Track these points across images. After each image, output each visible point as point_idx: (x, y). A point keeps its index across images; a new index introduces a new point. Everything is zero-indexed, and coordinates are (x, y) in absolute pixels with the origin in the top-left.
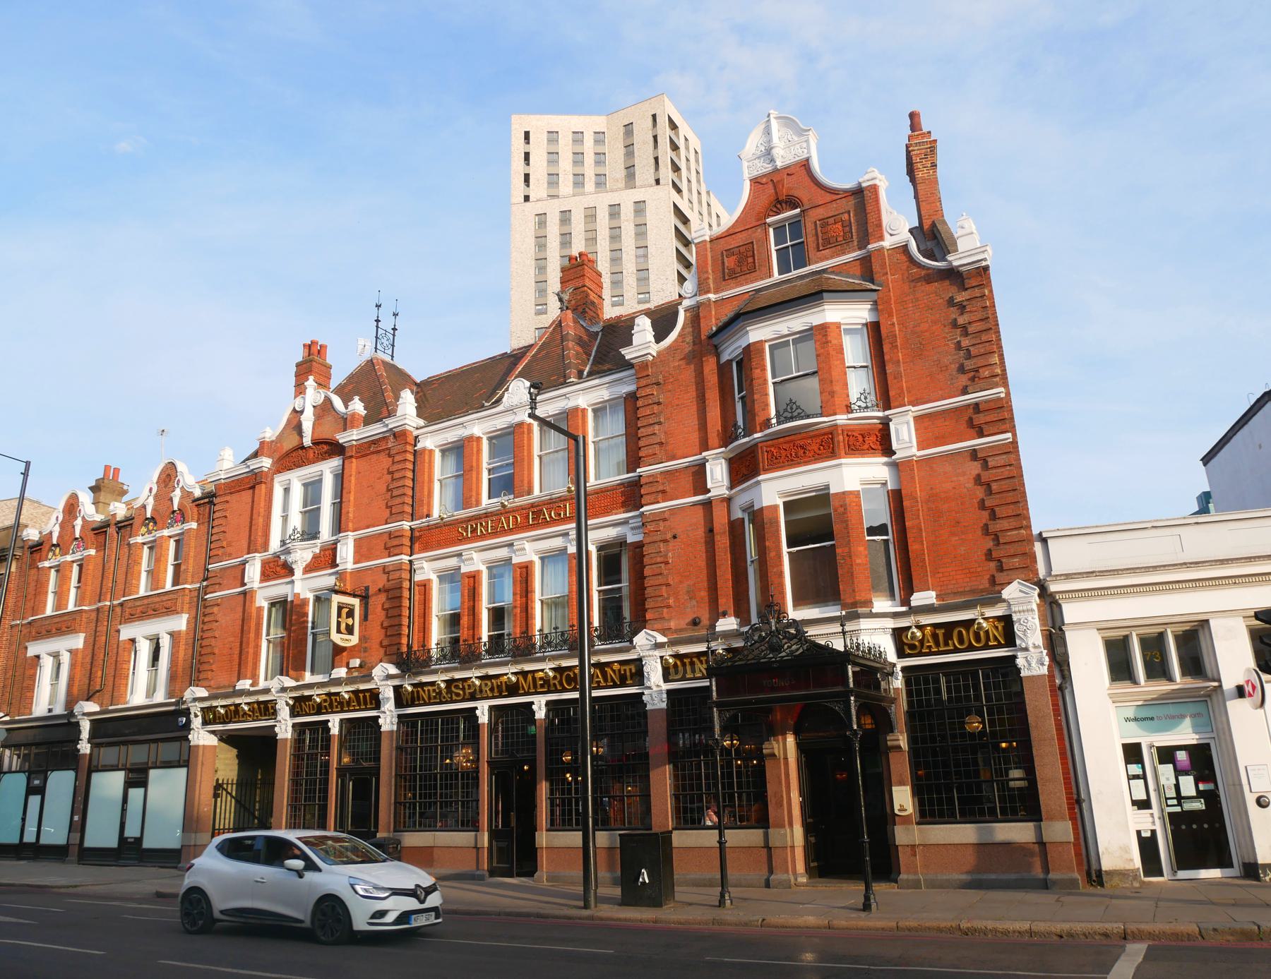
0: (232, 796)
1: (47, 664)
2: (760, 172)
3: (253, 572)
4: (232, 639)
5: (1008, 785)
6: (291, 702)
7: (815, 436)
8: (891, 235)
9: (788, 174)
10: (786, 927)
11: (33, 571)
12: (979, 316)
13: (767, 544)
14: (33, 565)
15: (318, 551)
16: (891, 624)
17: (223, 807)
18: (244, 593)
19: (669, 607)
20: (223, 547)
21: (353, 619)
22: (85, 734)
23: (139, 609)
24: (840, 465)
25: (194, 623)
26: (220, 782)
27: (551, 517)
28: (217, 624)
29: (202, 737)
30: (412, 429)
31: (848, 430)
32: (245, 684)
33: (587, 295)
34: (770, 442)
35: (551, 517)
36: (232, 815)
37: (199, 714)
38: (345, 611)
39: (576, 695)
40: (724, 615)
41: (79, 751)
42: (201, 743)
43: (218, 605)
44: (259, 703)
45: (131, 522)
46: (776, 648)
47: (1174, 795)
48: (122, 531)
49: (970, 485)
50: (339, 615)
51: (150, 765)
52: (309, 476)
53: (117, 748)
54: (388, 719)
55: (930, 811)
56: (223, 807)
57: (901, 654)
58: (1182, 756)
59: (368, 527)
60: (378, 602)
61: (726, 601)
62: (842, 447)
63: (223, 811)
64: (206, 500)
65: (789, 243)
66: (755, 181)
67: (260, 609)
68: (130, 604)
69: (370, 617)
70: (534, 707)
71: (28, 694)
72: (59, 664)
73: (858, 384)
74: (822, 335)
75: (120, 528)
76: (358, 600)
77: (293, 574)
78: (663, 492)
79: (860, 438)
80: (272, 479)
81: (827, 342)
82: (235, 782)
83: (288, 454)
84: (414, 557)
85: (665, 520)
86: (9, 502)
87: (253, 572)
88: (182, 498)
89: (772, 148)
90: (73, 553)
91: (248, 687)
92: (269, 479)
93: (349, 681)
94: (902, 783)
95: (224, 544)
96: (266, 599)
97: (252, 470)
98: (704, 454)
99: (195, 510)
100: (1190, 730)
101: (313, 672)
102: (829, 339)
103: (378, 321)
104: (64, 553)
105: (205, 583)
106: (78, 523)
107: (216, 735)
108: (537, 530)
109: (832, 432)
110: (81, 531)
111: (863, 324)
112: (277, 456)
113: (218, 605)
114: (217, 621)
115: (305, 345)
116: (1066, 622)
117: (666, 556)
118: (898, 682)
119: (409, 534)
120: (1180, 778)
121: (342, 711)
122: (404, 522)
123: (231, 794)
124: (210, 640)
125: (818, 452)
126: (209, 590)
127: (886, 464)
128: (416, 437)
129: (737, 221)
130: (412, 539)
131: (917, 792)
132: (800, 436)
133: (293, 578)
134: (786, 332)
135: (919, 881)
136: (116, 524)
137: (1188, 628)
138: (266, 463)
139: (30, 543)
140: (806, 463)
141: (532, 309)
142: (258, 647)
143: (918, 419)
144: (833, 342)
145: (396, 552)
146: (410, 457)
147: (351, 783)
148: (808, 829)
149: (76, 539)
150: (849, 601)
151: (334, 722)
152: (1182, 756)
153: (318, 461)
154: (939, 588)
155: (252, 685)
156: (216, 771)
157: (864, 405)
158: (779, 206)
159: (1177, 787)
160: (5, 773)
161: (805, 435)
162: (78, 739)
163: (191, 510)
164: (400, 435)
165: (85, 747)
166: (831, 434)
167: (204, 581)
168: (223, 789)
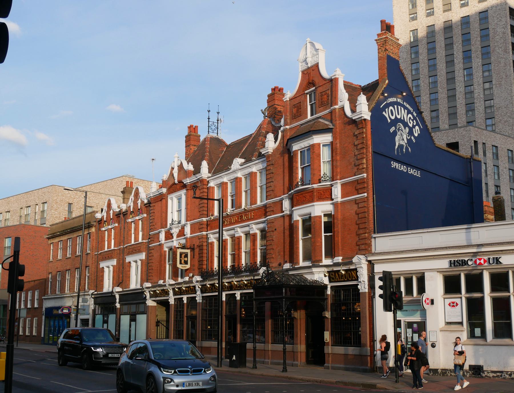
0: (164, 326)
1: (133, 265)
2: (304, 68)
3: (162, 236)
4: (157, 263)
5: (358, 333)
6: (200, 287)
7: (308, 193)
8: (341, 102)
9: (313, 70)
10: (253, 375)
11: (100, 232)
12: (361, 141)
13: (294, 236)
14: (99, 230)
15: (180, 229)
16: (326, 270)
17: (161, 330)
18: (160, 245)
19: (273, 258)
20: (154, 225)
21: (187, 258)
22: (118, 301)
23: (131, 250)
24: (314, 205)
25: (147, 256)
26: (159, 320)
27: (245, 218)
28: (153, 257)
29: (150, 303)
30: (206, 178)
31: (318, 190)
32: (161, 282)
33: (276, 109)
34: (297, 194)
35: (245, 218)
36: (165, 333)
37: (327, 275)
38: (183, 255)
39: (217, 294)
40: (286, 262)
41: (116, 306)
42: (150, 305)
43: (153, 249)
44: (333, 271)
45: (127, 213)
46: (224, 286)
47: (411, 341)
48: (125, 216)
49: (354, 214)
50: (181, 257)
51: (137, 313)
52: (178, 196)
53: (127, 306)
54: (199, 299)
55: (336, 342)
56: (161, 330)
57: (330, 281)
58: (415, 326)
59: (194, 220)
60: (197, 251)
61: (287, 258)
62: (315, 197)
63: (161, 331)
64: (148, 205)
65: (313, 102)
66: (303, 72)
67: (166, 251)
68: (128, 248)
69: (195, 257)
70: (236, 295)
71: (101, 283)
72: (138, 266)
73: (325, 169)
74: (313, 149)
75: (124, 215)
76: (190, 250)
77: (173, 238)
78: (273, 211)
79: (323, 193)
80: (167, 197)
81: (313, 152)
82: (165, 320)
83: (171, 186)
84: (208, 232)
85: (273, 223)
86: (119, 179)
87: (162, 236)
88: (141, 203)
89: (306, 58)
90: (111, 225)
91: (162, 283)
92: (166, 197)
93: (343, 264)
94: (327, 331)
95: (154, 224)
96: (167, 247)
97: (160, 193)
98: (282, 196)
99: (145, 209)
100: (419, 316)
101: (182, 277)
102: (314, 151)
103: (209, 119)
104: (109, 225)
105: (149, 240)
106: (111, 212)
107: (155, 302)
108: (250, 221)
109: (312, 191)
110: (112, 215)
111: (330, 142)
112: (168, 187)
113: (153, 249)
114: (153, 256)
115: (188, 127)
116: (375, 272)
117: (272, 237)
118: (329, 292)
119: (206, 223)
120: (414, 334)
121: (187, 294)
122: (203, 219)
123: (164, 325)
124: (151, 263)
125: (309, 199)
126: (151, 243)
127: (331, 204)
128: (208, 181)
129: (297, 91)
130: (207, 225)
131: (332, 334)
132: (304, 192)
133: (173, 240)
134: (303, 147)
135: (329, 366)
136: (122, 213)
137: (421, 275)
138: (164, 190)
139: (98, 220)
140: (306, 203)
141: (407, 17)
142: (165, 267)
143: (342, 185)
144: (316, 152)
145: (201, 231)
146: (206, 190)
147: (190, 322)
148: (308, 346)
149: (111, 219)
150: (314, 260)
151: (185, 298)
152: (415, 326)
153: (180, 190)
154: (343, 256)
155: (163, 282)
156: (157, 316)
157: (324, 179)
158: (310, 85)
159: (412, 337)
160: (97, 315)
161: (306, 192)
162: (115, 302)
163: (144, 209)
164: (201, 181)
165: (118, 305)
166: (313, 192)
167: (149, 239)
168: (160, 323)
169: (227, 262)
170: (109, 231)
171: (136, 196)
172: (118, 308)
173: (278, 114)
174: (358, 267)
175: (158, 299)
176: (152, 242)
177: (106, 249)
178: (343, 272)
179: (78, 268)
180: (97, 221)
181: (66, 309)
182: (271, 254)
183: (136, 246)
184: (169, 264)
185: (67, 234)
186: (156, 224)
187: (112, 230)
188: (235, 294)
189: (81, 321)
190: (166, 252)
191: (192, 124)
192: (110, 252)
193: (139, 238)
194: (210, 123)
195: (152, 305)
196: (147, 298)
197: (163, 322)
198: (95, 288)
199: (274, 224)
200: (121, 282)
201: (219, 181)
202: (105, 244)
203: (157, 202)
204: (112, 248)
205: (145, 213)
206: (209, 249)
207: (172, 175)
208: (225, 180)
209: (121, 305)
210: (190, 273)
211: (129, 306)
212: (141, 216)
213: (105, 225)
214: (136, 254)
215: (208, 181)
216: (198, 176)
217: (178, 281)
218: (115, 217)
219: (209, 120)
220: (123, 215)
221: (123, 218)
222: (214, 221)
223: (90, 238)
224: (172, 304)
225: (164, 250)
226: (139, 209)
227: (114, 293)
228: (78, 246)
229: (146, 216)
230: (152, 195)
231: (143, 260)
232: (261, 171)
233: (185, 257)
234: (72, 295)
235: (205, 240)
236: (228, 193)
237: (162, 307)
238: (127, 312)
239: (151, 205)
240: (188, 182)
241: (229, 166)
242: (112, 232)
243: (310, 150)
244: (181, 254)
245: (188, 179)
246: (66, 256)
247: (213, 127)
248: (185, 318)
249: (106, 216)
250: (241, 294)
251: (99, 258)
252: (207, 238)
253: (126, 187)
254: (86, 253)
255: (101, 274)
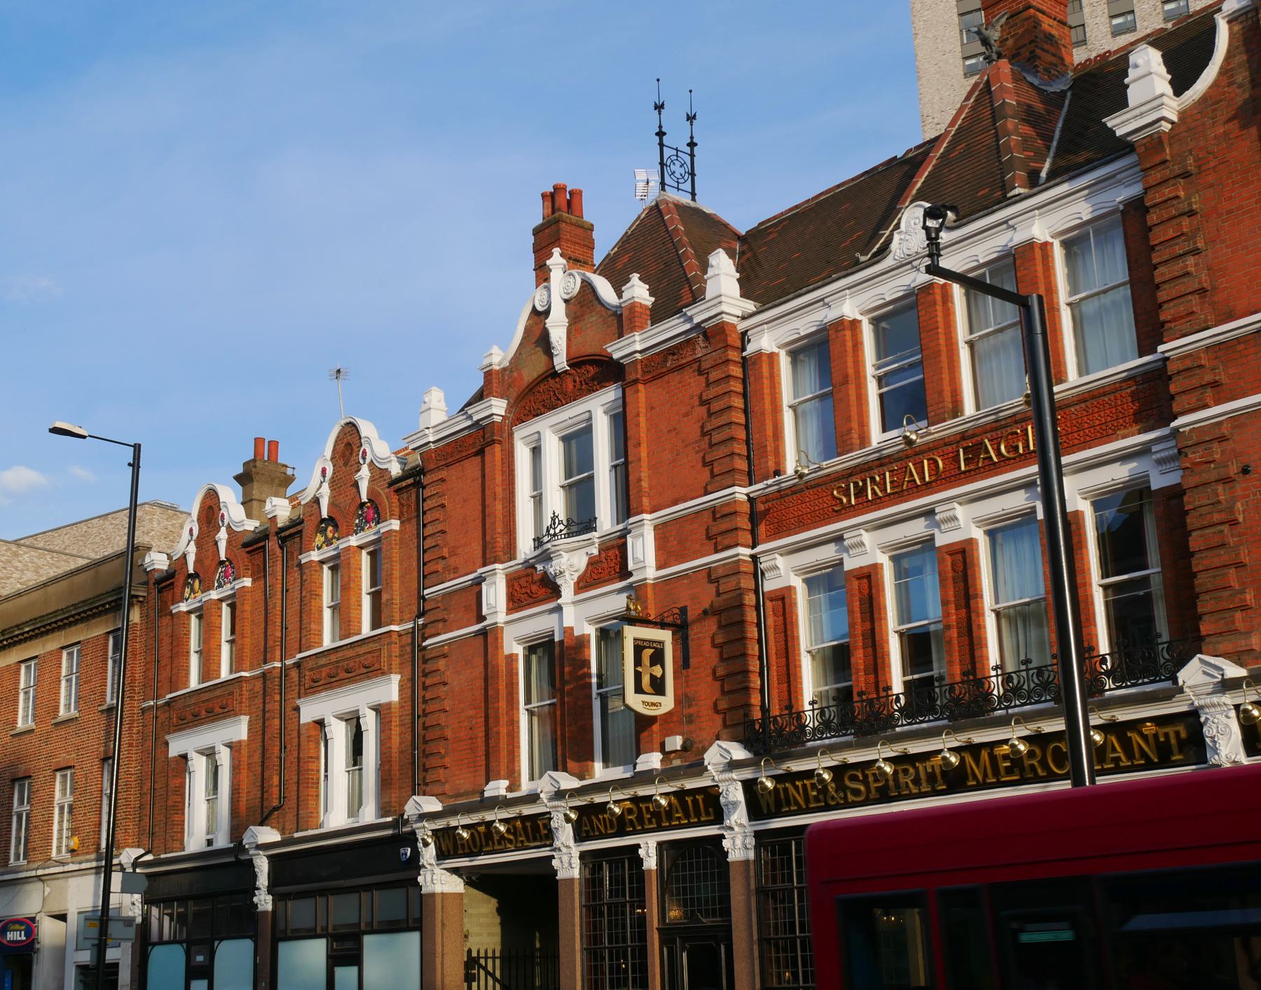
1: (199, 765)
3: (495, 595)
4: (471, 713)
6: (573, 816)
11: (166, 620)
14: (164, 611)
15: (595, 552)
18: (484, 633)
20: (443, 558)
21: (663, 667)
22: (263, 880)
23: (325, 671)
25: (410, 688)
28: (446, 688)
30: (734, 320)
33: (1037, 24)
38: (648, 653)
42: (438, 889)
45: (299, 528)
48: (288, 543)
50: (638, 661)
51: (363, 927)
52: (570, 422)
59: (675, 503)
60: (704, 633)
64: (410, 481)
67: (512, 658)
71: (176, 818)
72: (217, 767)
75: (284, 540)
78: (1215, 385)
80: (511, 435)
82: (498, 954)
84: (759, 548)
85: (1222, 439)
87: (495, 595)
88: (372, 480)
90: (220, 586)
91: (503, 792)
92: (506, 435)
93: (667, 774)
95: (445, 552)
96: (520, 640)
99: (395, 498)
101: (606, 761)
103: (661, 134)
104: (207, 588)
105: (421, 621)
106: (222, 535)
107: (460, 876)
112: (514, 393)
113: (444, 656)
114: (445, 684)
115: (544, 196)
117: (1231, 510)
119: (746, 508)
121: (660, 828)
122: (737, 489)
123: (493, 975)
126: (428, 631)
128: (744, 333)
130: (754, 518)
136: (277, 533)
138: (498, 407)
139: (156, 575)
142: (513, 724)
146: (737, 371)
147: (685, 955)
149: (222, 563)
151: (648, 847)
155: (509, 789)
160: (154, 944)
162: (252, 888)
163: (388, 500)
164: (715, 333)
165: (264, 901)
167: (419, 616)
168: (480, 966)
169: (889, 666)
170: (201, 612)
171: (343, 456)
172: (266, 912)
173: (1046, 47)
174: (418, 828)
175: (463, 862)
176: (441, 625)
177: (194, 683)
178: (888, 769)
179: (110, 758)
180: (153, 581)
181: (17, 927)
182: (1226, 593)
183: (350, 653)
184: (531, 713)
185: (20, 642)
186: (453, 553)
187: (220, 609)
188: (638, 846)
189: (81, 973)
190: (517, 660)
191: (560, 181)
192: (218, 692)
193: (360, 622)
194: (667, 152)
195: (448, 889)
196: (422, 861)
197: (490, 962)
198: (145, 841)
199: (1228, 446)
200: (275, 803)
201: (805, 325)
202: (188, 667)
203: (459, 461)
204: (225, 674)
205: (392, 516)
206: (770, 621)
207: (538, 338)
208: (850, 308)
209: (278, 898)
210: (672, 733)
211: (365, 896)
212: (375, 530)
213: (187, 590)
214: (352, 687)
215: (744, 333)
216: (699, 313)
217: (592, 777)
218: (242, 554)
219: (661, 140)
220: (282, 539)
221: (278, 551)
222: (794, 493)
223: (117, 648)
224: (572, 880)
225: (506, 652)
226: (362, 505)
227: (245, 851)
228: (63, 684)
229: (397, 528)
230: (432, 439)
231: (240, 742)
232: (1074, 243)
233: (653, 664)
234: (40, 872)
235: (748, 583)
236: (864, 366)
237: (485, 896)
238: (404, 916)
239: (425, 480)
240: (638, 347)
241: (857, 255)
242: (220, 616)
243: (380, 541)
244: (639, 648)
245: (637, 338)
246: (14, 728)
247: (679, 170)
248: (654, 940)
249: (197, 555)
250: (660, 845)
251: (160, 720)
252: (757, 574)
253: (254, 461)
254: (53, 721)
255: (174, 783)
